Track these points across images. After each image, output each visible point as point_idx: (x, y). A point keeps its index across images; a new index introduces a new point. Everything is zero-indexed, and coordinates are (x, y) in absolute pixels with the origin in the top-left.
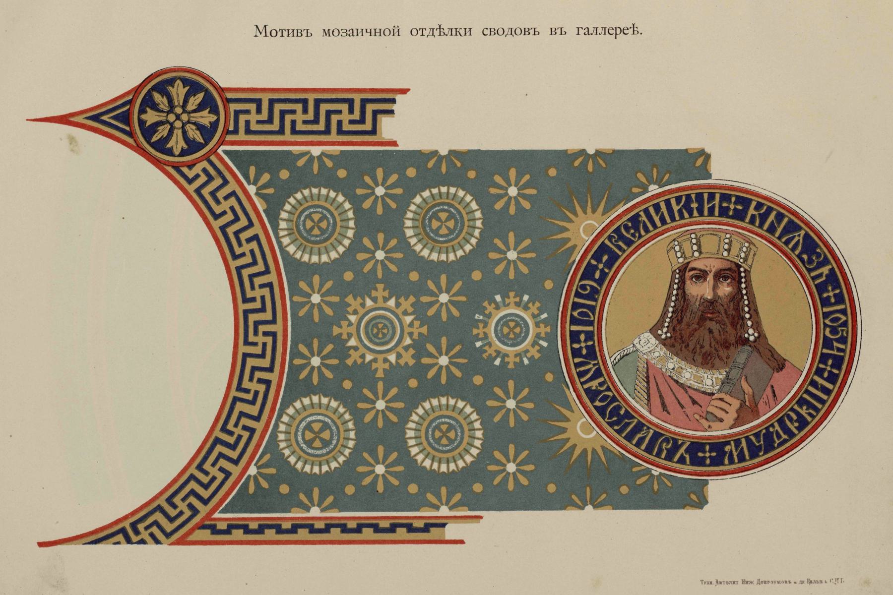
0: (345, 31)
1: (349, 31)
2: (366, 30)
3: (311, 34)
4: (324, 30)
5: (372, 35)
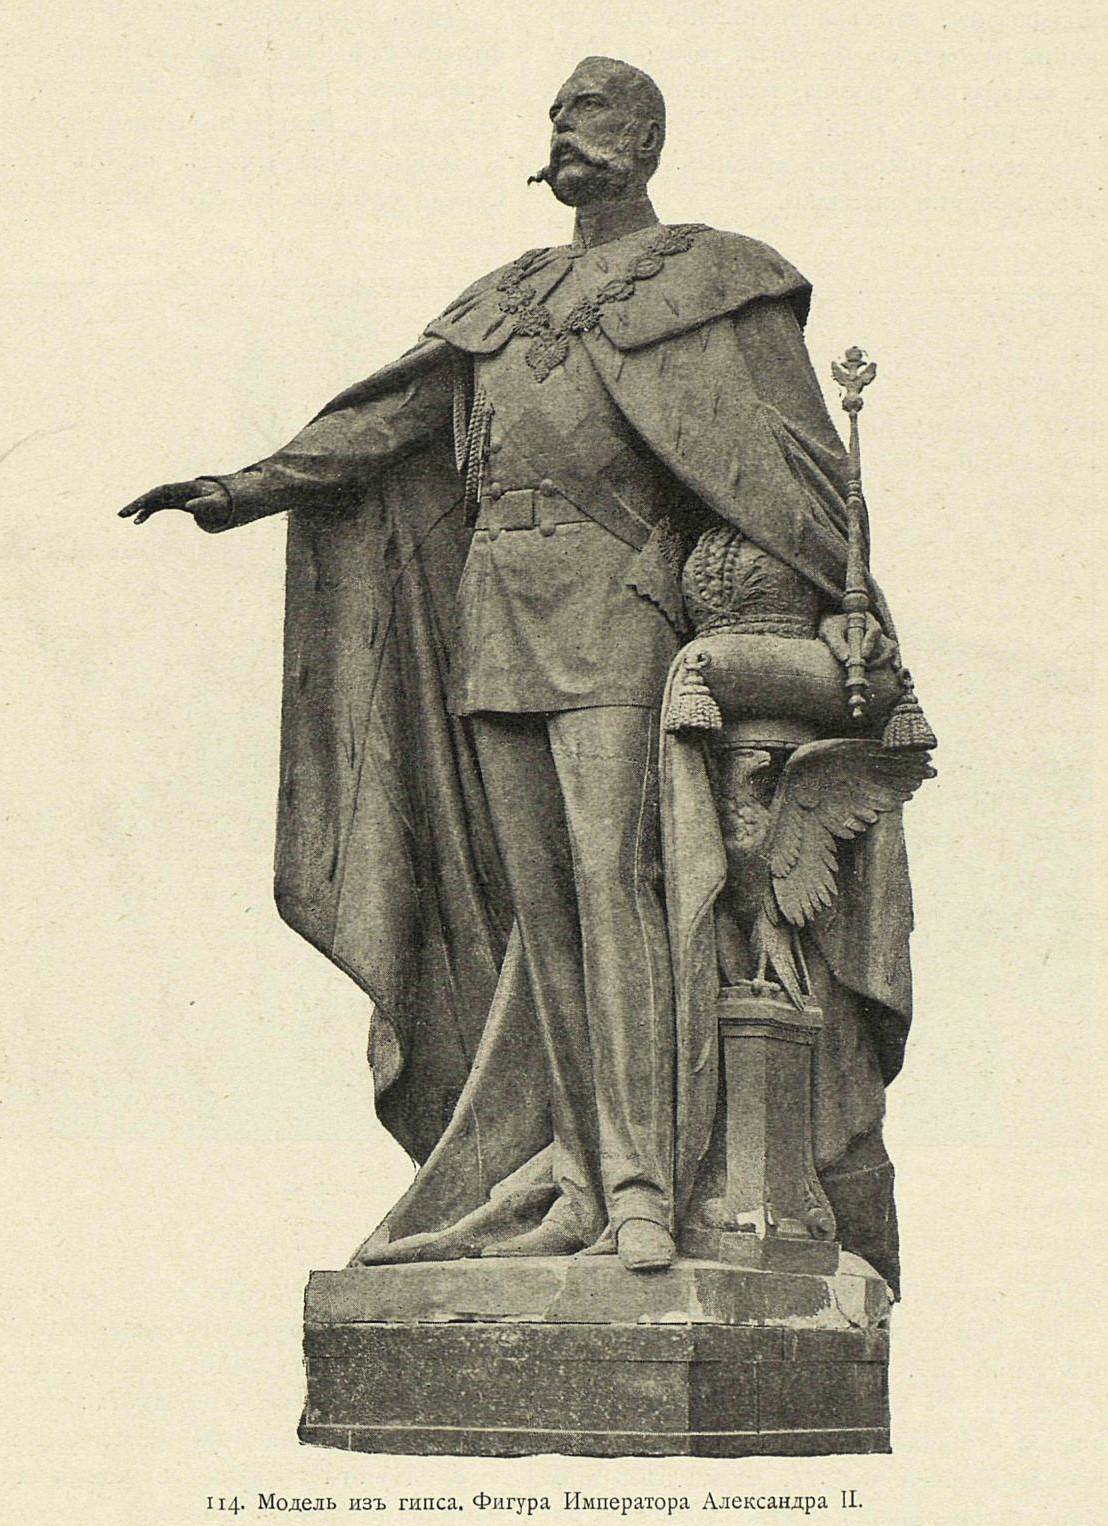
0: (367, 1501)
3: (335, 1506)
4: (262, 1496)
5: (850, 1494)
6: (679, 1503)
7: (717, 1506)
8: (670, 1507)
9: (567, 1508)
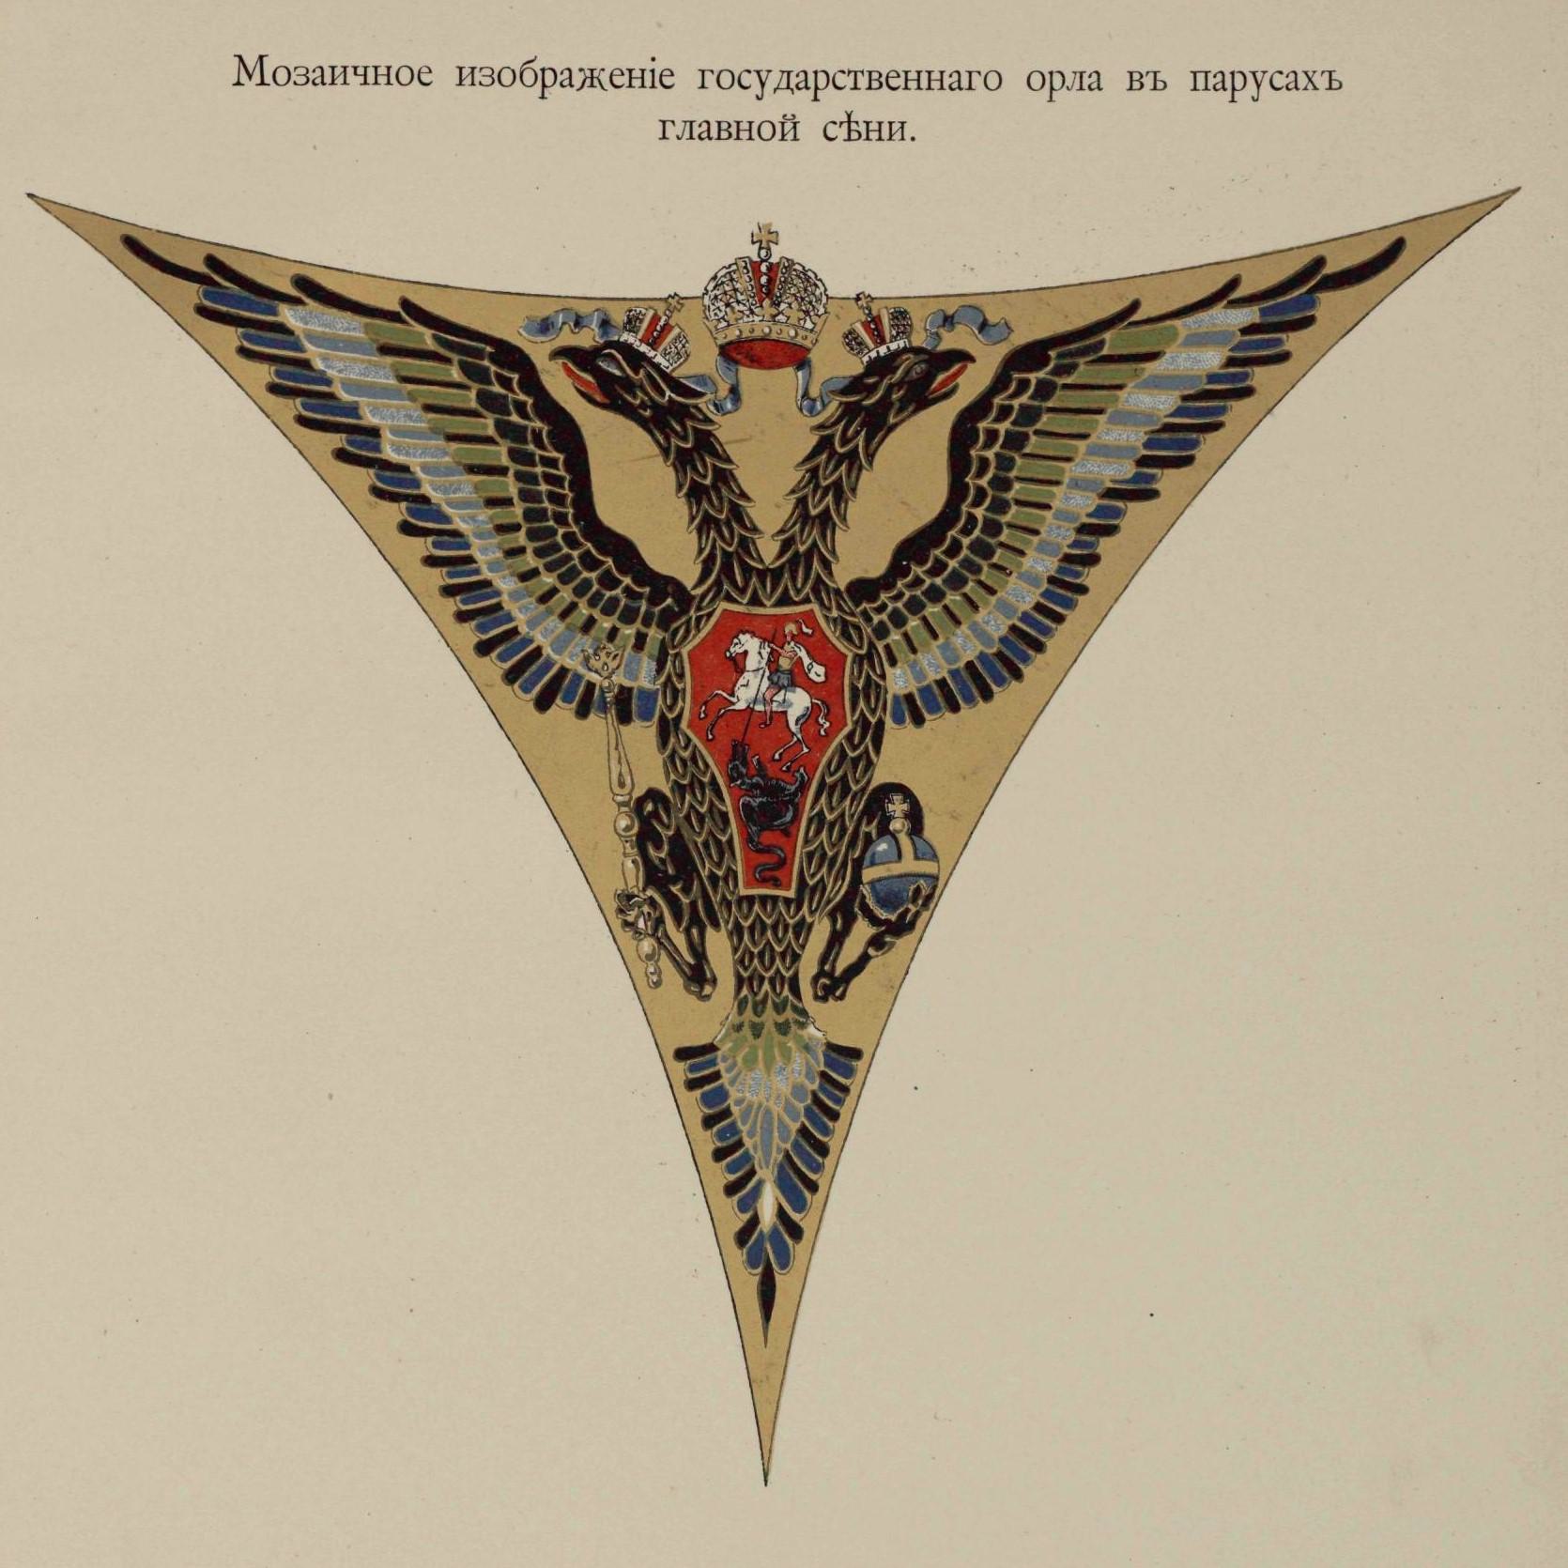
0: (304, 71)
1: (314, 71)
2: (355, 68)
6: (560, 78)
7: (755, 74)
8: (1052, 89)
9: (903, 123)
